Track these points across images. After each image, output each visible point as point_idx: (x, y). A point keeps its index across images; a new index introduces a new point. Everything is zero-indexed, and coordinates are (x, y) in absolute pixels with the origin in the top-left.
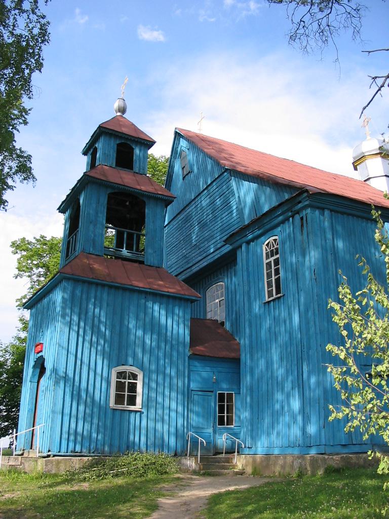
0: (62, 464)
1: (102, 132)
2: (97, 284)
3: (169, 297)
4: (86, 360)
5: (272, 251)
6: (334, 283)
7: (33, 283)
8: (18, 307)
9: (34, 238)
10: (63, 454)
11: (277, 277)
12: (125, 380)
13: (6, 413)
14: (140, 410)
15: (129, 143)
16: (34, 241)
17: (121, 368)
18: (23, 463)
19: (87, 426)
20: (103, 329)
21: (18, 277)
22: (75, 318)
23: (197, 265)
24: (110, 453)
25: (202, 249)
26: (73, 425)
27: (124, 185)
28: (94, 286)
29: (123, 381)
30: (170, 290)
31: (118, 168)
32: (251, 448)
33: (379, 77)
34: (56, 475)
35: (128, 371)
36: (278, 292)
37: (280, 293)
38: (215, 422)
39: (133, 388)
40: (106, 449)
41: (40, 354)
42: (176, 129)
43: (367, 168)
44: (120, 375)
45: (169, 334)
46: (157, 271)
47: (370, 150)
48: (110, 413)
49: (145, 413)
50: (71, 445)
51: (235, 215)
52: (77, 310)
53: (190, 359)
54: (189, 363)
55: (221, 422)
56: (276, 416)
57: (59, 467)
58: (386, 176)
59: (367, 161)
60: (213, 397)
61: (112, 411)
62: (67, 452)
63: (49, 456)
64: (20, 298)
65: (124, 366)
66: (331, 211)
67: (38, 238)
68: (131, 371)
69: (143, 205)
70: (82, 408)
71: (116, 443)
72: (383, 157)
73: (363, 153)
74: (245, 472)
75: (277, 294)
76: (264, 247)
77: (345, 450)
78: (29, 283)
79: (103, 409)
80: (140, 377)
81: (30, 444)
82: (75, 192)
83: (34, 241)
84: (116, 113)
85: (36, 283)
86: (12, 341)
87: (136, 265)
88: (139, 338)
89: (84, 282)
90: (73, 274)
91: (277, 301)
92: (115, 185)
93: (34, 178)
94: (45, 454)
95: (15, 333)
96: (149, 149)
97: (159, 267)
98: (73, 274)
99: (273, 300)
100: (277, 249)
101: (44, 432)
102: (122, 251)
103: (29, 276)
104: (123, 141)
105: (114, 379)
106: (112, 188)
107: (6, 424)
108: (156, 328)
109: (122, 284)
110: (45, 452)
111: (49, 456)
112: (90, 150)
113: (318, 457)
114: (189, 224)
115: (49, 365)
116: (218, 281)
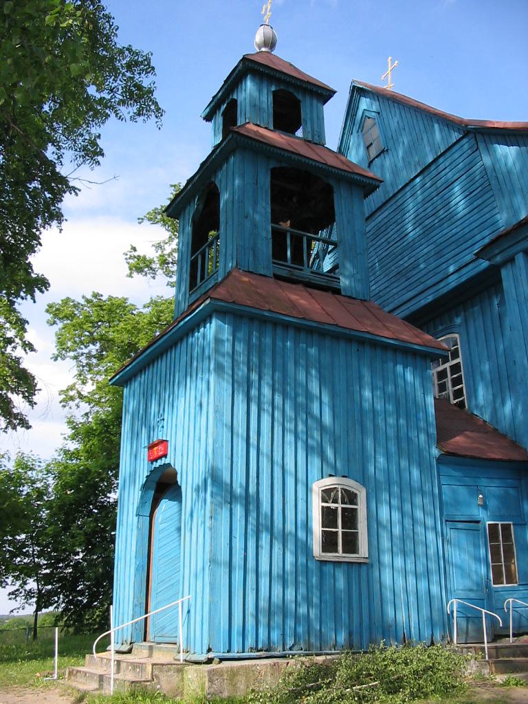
0: (239, 678)
1: (248, 68)
4: (290, 466)
7: (81, 368)
8: (63, 404)
9: (83, 297)
12: (336, 505)
13: (48, 571)
16: (83, 302)
18: (157, 677)
21: (59, 358)
24: (321, 648)
29: (333, 506)
35: (339, 487)
41: (160, 463)
42: (353, 82)
54: (438, 472)
57: (236, 684)
61: (318, 563)
62: (243, 652)
63: (210, 661)
64: (65, 389)
67: (89, 297)
69: (328, 192)
70: (290, 558)
78: (75, 368)
83: (83, 302)
85: (85, 368)
86: (56, 455)
87: (329, 294)
93: (158, 109)
94: (203, 657)
95: (60, 443)
96: (324, 104)
97: (365, 300)
101: (189, 612)
102: (301, 270)
103: (76, 358)
104: (282, 87)
107: (50, 587)
109: (320, 323)
111: (210, 661)
114: (383, 240)
115: (189, 476)
116: (449, 331)
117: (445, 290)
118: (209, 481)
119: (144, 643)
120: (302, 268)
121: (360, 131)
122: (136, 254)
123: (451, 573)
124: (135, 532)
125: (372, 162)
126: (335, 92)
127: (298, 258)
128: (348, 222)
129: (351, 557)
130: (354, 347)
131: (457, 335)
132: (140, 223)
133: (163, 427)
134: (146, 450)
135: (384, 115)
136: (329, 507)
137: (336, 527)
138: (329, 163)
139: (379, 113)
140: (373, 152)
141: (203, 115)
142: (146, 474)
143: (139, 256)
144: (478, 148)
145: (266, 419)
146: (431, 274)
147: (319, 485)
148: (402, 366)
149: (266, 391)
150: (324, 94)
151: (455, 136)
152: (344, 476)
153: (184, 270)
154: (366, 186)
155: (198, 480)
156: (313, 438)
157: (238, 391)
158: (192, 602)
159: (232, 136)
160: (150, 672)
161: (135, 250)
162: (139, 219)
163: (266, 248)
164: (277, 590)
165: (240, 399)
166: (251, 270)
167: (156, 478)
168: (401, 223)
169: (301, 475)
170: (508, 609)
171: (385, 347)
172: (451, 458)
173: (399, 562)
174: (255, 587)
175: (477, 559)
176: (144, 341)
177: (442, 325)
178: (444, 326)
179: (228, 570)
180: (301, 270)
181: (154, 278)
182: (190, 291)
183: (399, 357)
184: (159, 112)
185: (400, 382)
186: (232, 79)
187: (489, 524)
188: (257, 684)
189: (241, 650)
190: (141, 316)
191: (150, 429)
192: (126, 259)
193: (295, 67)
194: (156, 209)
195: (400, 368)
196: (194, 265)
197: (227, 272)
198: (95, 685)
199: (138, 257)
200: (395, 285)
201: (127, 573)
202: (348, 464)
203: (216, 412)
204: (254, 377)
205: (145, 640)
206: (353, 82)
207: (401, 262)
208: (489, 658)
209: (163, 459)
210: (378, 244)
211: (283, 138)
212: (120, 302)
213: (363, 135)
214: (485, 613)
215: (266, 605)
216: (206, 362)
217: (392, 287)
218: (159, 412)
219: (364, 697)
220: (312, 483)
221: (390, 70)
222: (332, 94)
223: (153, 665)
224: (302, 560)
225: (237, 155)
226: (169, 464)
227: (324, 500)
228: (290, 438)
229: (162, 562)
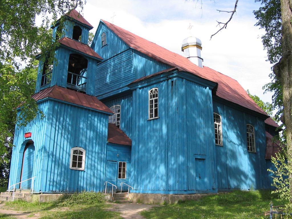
1: (66, 18)
2: (65, 104)
3: (99, 112)
4: (59, 143)
6: (185, 115)
11: (156, 108)
12: (77, 155)
14: (84, 170)
17: (75, 149)
18: (26, 197)
19: (59, 178)
22: (55, 120)
23: (106, 95)
25: (110, 87)
26: (52, 177)
27: (79, 51)
28: (64, 105)
29: (76, 155)
30: (101, 109)
31: (73, 40)
33: (222, 23)
34: (45, 203)
35: (78, 150)
36: (156, 115)
38: (117, 177)
39: (80, 158)
40: (68, 189)
41: (28, 138)
42: (101, 20)
43: (189, 52)
44: (75, 152)
45: (98, 130)
46: (92, 97)
48: (69, 173)
49: (86, 171)
50: (51, 187)
51: (132, 72)
52: (55, 116)
55: (120, 177)
56: (150, 176)
58: (198, 57)
59: (189, 48)
60: (117, 164)
63: (40, 193)
65: (77, 147)
66: (186, 80)
71: (72, 186)
72: (197, 47)
73: (188, 43)
74: (133, 202)
75: (155, 117)
76: (149, 92)
77: (186, 193)
79: (66, 168)
80: (84, 153)
88: (84, 132)
94: (39, 192)
97: (93, 96)
99: (153, 119)
100: (157, 94)
104: (77, 25)
105: (72, 154)
106: (72, 51)
108: (93, 128)
109: (78, 105)
110: (37, 190)
111: (40, 193)
113: (175, 196)
115: (38, 145)
118: (43, 149)
126: (93, 28)
127: (74, 83)
128: (91, 72)
136: (75, 155)
146: (114, 87)
154: (98, 61)
155: (40, 147)
163: (65, 77)
166: (60, 86)
167: (26, 142)
182: (41, 86)
187: (73, 166)
189: (48, 191)
198: (5, 200)
203: (47, 128)
205: (19, 188)
206: (101, 20)
209: (30, 138)
210: (101, 73)
217: (104, 87)
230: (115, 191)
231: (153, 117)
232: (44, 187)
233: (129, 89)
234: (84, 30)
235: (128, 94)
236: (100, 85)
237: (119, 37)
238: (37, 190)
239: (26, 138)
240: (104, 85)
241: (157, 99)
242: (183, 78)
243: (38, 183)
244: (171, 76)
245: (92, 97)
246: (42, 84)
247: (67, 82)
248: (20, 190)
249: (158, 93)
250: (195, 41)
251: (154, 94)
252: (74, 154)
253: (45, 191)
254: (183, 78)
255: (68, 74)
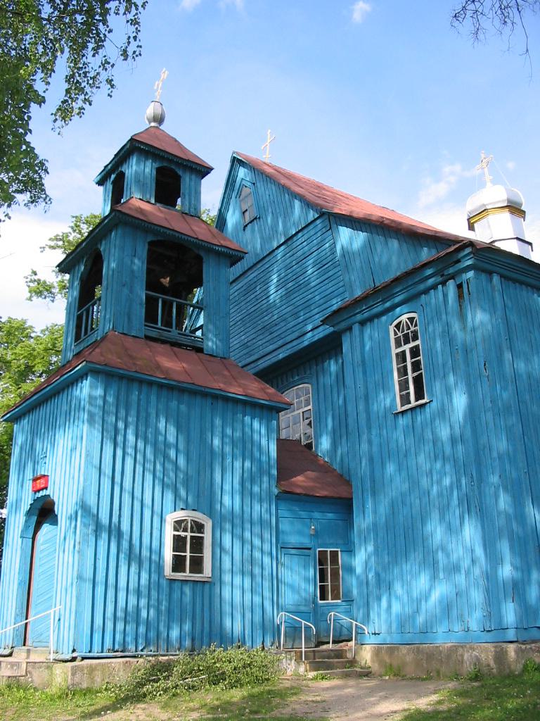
1: (135, 148)
5: (406, 336)
10: (96, 655)
11: (416, 374)
12: (186, 534)
14: (210, 580)
15: (173, 167)
18: (30, 673)
20: (172, 453)
27: (173, 230)
28: (136, 385)
29: (183, 534)
31: (158, 205)
32: (379, 634)
34: (88, 692)
35: (189, 519)
36: (419, 395)
37: (424, 398)
42: (234, 153)
43: (489, 226)
47: (494, 201)
48: (164, 583)
53: (278, 499)
58: (517, 239)
59: (490, 217)
61: (168, 582)
62: (102, 652)
63: (74, 659)
65: (194, 512)
66: (502, 276)
68: (194, 519)
69: (199, 261)
70: (144, 576)
72: (512, 213)
73: (484, 205)
76: (392, 328)
81: (23, 637)
82: (92, 238)
84: (150, 123)
89: (121, 377)
90: (106, 365)
91: (418, 410)
92: (159, 228)
94: (69, 657)
98: (106, 365)
99: (411, 409)
101: (59, 620)
102: (170, 331)
104: (165, 164)
106: (155, 233)
110: (65, 650)
111: (74, 659)
112: (113, 177)
114: (252, 296)
115: (63, 509)
117: (302, 347)
119: (23, 647)
120: (171, 330)
121: (238, 197)
122: (36, 278)
123: (283, 591)
124: (19, 552)
125: (246, 226)
126: (212, 169)
128: (214, 289)
129: (196, 577)
130: (209, 401)
131: (310, 386)
132: (42, 252)
133: (45, 463)
134: (31, 482)
135: (258, 184)
136: (179, 536)
137: (185, 552)
138: (200, 237)
139: (254, 184)
140: (248, 218)
141: (96, 181)
142: (30, 502)
143: (39, 280)
144: (330, 228)
145: (129, 461)
146: (289, 332)
147: (171, 517)
148: (250, 418)
149: (131, 438)
150: (202, 170)
151: (312, 215)
152: (193, 510)
153: (71, 323)
154: (233, 257)
155: (71, 511)
156: (169, 478)
157: (107, 439)
158: (62, 612)
159: (115, 214)
160: (25, 669)
161: (36, 274)
162: (41, 248)
163: (140, 312)
164: (133, 600)
165: (108, 449)
166: (125, 332)
167: (39, 505)
168: (267, 282)
169: (157, 508)
170: (330, 620)
171: (236, 401)
172: (287, 496)
173: (237, 580)
174: (114, 600)
175: (307, 580)
176: (40, 365)
177: (298, 375)
178: (300, 376)
179: (92, 586)
180: (170, 331)
181: (53, 301)
183: (248, 409)
184: (47, 200)
185: (247, 430)
186: (121, 154)
188: (111, 678)
190: (38, 340)
191: (35, 463)
192: (27, 282)
193: (179, 143)
194: (58, 235)
195: (247, 419)
196: (79, 318)
197: (105, 332)
199: (39, 282)
200: (261, 337)
201: (11, 587)
202: (198, 500)
203: (87, 456)
204: (121, 425)
205: (24, 645)
206: (234, 153)
207: (266, 318)
208: (305, 659)
209: (45, 490)
210: (248, 299)
211: (162, 212)
212: (18, 325)
213: (240, 201)
214: (305, 624)
215: (123, 615)
216: (82, 413)
218: (43, 450)
219: (193, 687)
220: (166, 515)
221: (269, 141)
222: (209, 170)
223: (27, 663)
224: (154, 577)
225: (120, 231)
226: (49, 496)
227: (176, 529)
228: (149, 477)
229: (42, 577)
230: (313, 639)
231: (410, 403)
232: (86, 639)
233: (332, 329)
234: (187, 180)
235: (329, 347)
236: (248, 335)
237: (283, 186)
238: (65, 650)
239: (35, 493)
240: (259, 332)
241: (417, 347)
242: (490, 273)
243: (67, 625)
244: (451, 270)
245: (223, 363)
246: (77, 337)
247: (146, 321)
248: (29, 651)
249: (418, 328)
250: (505, 197)
251: (406, 332)
252: (177, 533)
253: (90, 652)
254: (490, 273)
255: (147, 297)
